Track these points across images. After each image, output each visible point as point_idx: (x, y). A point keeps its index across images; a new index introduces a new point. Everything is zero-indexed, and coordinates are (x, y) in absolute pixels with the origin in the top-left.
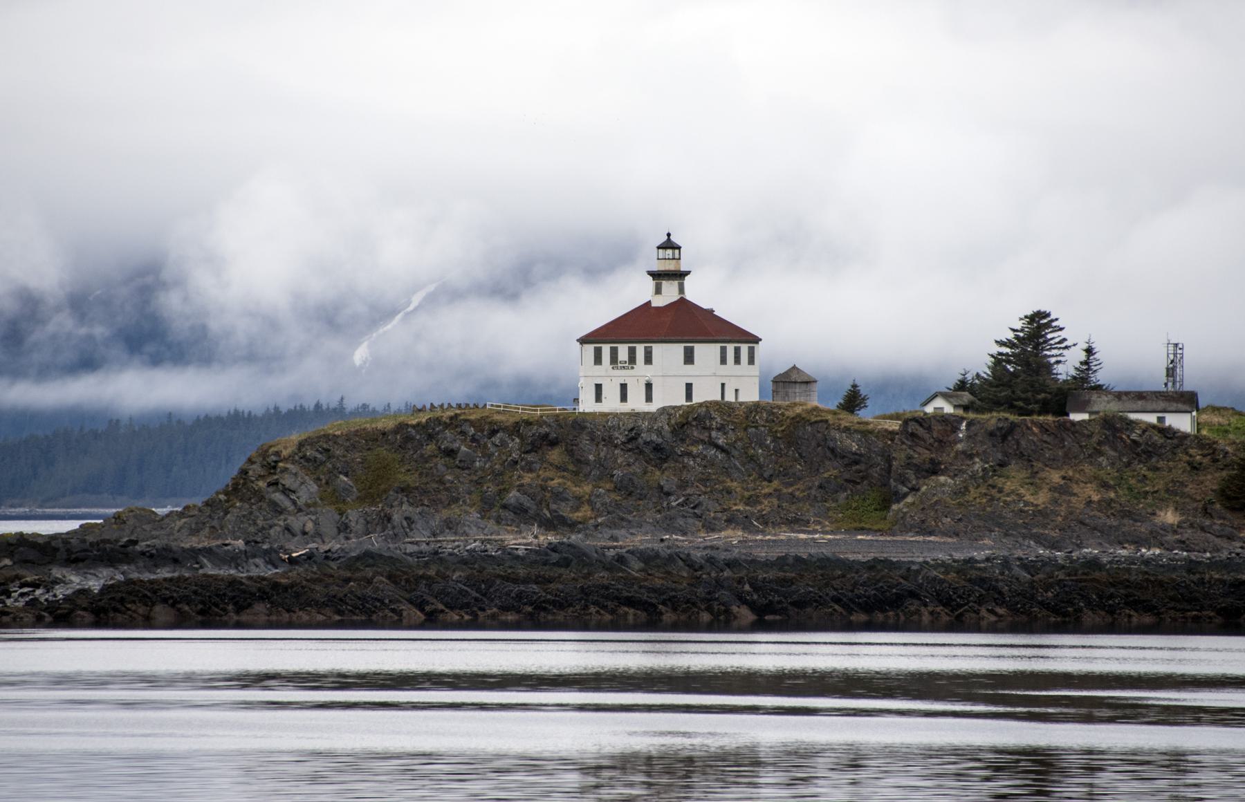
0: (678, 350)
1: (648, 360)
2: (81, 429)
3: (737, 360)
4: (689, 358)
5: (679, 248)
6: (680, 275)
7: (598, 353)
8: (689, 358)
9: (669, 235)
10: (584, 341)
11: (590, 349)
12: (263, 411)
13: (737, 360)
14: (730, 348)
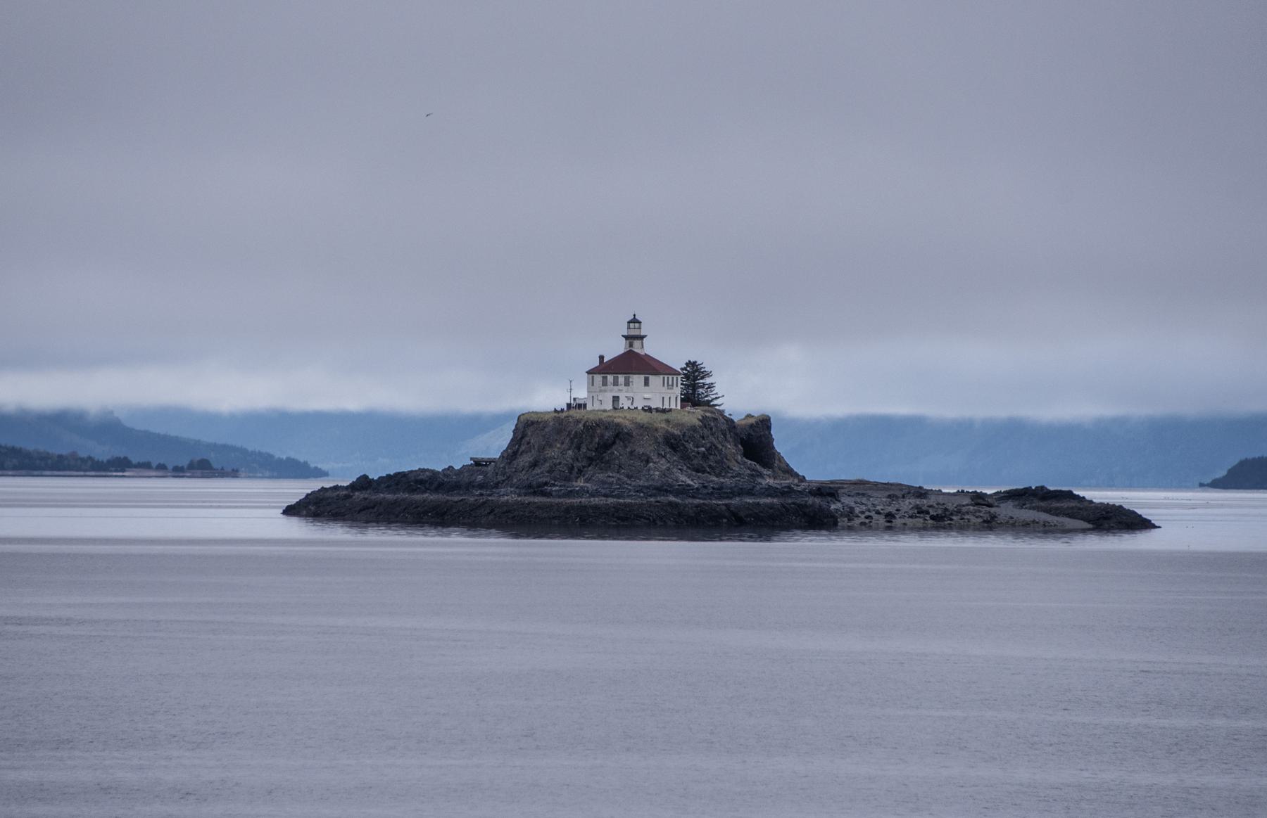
3: (616, 383)
4: (647, 383)
8: (647, 383)
10: (589, 373)
13: (616, 383)
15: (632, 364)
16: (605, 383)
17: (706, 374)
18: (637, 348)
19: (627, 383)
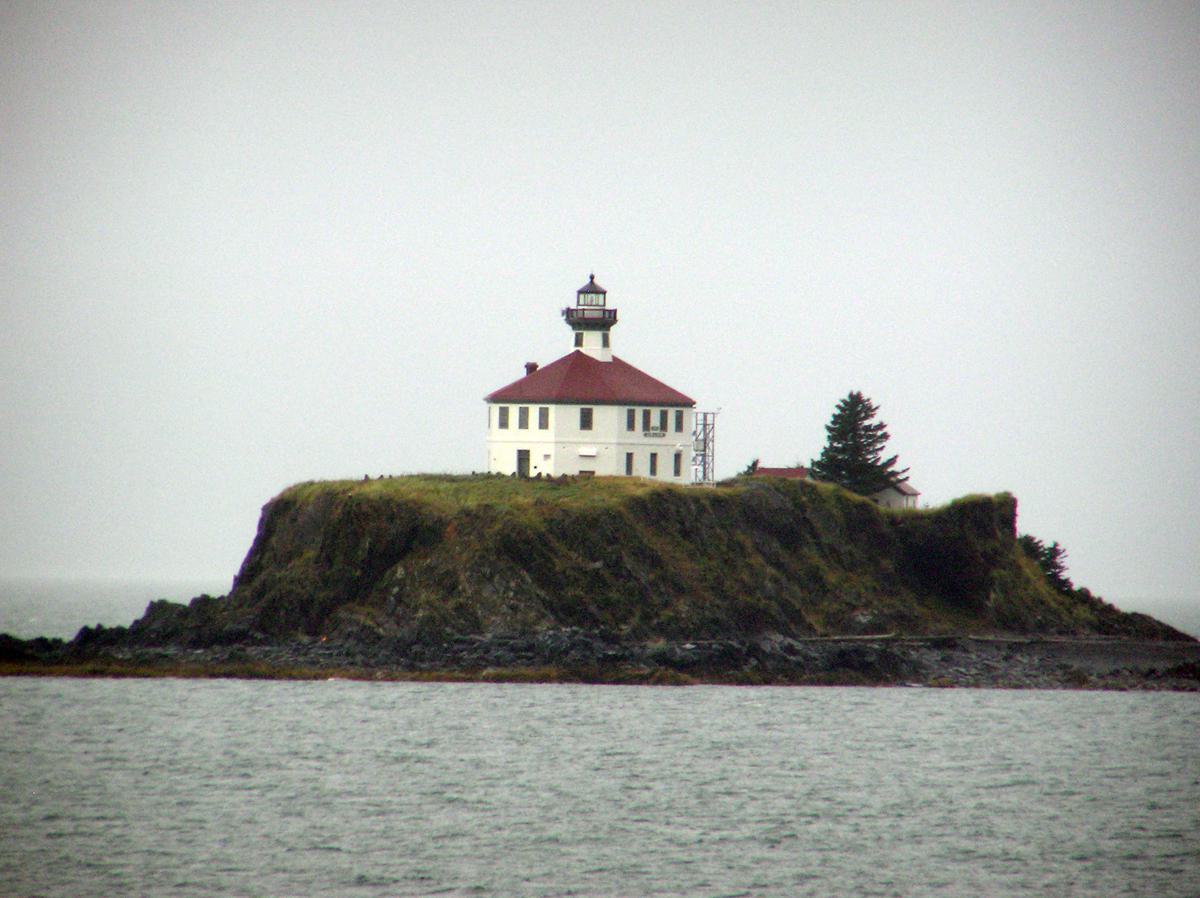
0: (574, 412)
1: (543, 424)
2: (892, 461)
3: (523, 423)
4: (586, 422)
5: (604, 293)
6: (604, 322)
7: (504, 413)
8: (586, 422)
9: (592, 277)
10: (495, 398)
11: (496, 408)
12: (320, 490)
13: (523, 423)
14: (639, 412)
15: (579, 382)
16: (504, 424)
17: (869, 411)
19: (543, 424)
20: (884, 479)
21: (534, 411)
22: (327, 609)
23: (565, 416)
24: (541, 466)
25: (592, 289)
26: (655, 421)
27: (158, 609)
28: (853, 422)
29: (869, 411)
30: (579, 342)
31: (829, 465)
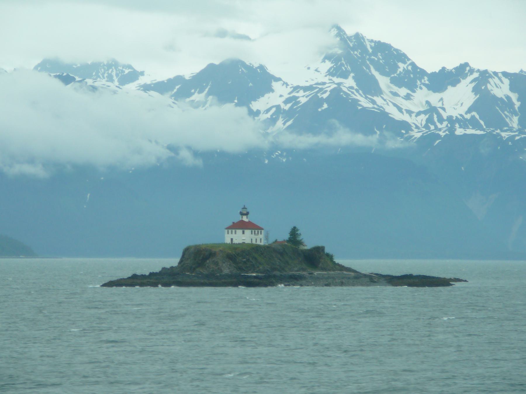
1: (235, 233)
3: (232, 233)
4: (243, 233)
8: (243, 233)
13: (232, 233)
16: (228, 233)
17: (297, 230)
18: (245, 219)
19: (235, 233)
20: (300, 243)
21: (234, 231)
22: (194, 269)
23: (239, 232)
24: (235, 241)
25: (244, 208)
26: (256, 232)
27: (164, 269)
28: (294, 232)
29: (297, 230)
30: (242, 218)
31: (290, 241)
